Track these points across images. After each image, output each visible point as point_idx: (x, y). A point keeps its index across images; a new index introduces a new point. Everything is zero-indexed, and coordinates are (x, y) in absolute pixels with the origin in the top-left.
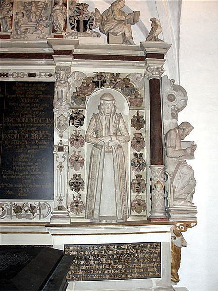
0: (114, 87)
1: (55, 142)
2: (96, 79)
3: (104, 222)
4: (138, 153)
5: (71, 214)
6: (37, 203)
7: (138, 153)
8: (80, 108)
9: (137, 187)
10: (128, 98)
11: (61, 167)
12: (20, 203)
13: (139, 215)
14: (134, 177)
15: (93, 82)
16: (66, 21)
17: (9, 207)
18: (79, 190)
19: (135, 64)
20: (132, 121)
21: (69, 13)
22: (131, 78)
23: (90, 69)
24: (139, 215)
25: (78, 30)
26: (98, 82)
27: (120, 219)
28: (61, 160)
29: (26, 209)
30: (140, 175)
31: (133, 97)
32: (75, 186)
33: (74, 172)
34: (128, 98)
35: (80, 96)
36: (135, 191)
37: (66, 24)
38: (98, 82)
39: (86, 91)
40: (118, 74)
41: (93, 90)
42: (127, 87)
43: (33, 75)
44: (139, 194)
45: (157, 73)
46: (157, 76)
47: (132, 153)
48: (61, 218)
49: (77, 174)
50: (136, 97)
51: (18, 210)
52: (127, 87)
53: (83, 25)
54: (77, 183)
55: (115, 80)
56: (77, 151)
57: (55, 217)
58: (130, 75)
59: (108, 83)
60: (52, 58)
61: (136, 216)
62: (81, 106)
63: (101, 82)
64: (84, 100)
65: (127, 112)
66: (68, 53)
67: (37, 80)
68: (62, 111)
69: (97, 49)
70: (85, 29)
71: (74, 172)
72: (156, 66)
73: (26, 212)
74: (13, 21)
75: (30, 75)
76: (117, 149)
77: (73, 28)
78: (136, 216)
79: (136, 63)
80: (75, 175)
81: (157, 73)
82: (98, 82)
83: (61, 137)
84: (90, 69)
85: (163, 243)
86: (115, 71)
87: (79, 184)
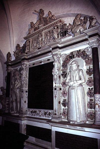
0: (78, 57)
1: (54, 86)
2: (71, 55)
3: (71, 123)
4: (91, 88)
5: (63, 117)
6: (51, 111)
7: (91, 88)
8: (65, 70)
9: (90, 106)
10: (85, 60)
11: (55, 97)
12: (46, 111)
13: (92, 121)
14: (89, 100)
15: (70, 57)
16: (58, 34)
17: (43, 112)
18: (66, 106)
19: (85, 43)
20: (87, 72)
21: (59, 31)
22: (86, 50)
23: (68, 52)
24: (92, 121)
25: (63, 36)
26: (71, 56)
27: (79, 122)
28: (55, 93)
29: (48, 113)
30: (92, 99)
31: (87, 59)
32: (64, 105)
33: (64, 98)
34: (85, 60)
35: (65, 65)
36: (89, 107)
37: (58, 35)
38: (71, 56)
39: (67, 61)
40: (80, 50)
41: (69, 61)
42: (84, 55)
43: (41, 62)
44: (92, 110)
45: (94, 44)
46: (95, 46)
47: (88, 88)
48: (55, 119)
49: (65, 99)
50: (88, 59)
51: (45, 114)
52: (84, 55)
53: (64, 33)
54: (65, 103)
55: (79, 53)
56: (65, 88)
57: (53, 118)
58: (85, 49)
59: (75, 56)
60: (51, 52)
61: (90, 121)
62: (65, 69)
63: (73, 56)
64: (66, 66)
65: (85, 68)
66: (57, 47)
67: (50, 62)
68: (56, 72)
69: (68, 42)
70: (65, 35)
71: (64, 98)
72: (93, 41)
73: (48, 115)
74: (43, 41)
75: (34, 64)
76: (77, 87)
77: (61, 36)
78: (90, 121)
79: (86, 42)
80: (64, 100)
81: (94, 44)
82: (71, 56)
83: (56, 84)
84: (68, 52)
85: (99, 139)
86: (78, 49)
87: (65, 104)
